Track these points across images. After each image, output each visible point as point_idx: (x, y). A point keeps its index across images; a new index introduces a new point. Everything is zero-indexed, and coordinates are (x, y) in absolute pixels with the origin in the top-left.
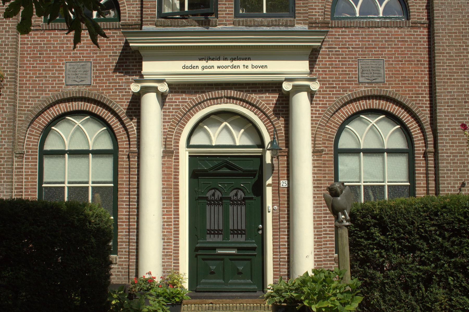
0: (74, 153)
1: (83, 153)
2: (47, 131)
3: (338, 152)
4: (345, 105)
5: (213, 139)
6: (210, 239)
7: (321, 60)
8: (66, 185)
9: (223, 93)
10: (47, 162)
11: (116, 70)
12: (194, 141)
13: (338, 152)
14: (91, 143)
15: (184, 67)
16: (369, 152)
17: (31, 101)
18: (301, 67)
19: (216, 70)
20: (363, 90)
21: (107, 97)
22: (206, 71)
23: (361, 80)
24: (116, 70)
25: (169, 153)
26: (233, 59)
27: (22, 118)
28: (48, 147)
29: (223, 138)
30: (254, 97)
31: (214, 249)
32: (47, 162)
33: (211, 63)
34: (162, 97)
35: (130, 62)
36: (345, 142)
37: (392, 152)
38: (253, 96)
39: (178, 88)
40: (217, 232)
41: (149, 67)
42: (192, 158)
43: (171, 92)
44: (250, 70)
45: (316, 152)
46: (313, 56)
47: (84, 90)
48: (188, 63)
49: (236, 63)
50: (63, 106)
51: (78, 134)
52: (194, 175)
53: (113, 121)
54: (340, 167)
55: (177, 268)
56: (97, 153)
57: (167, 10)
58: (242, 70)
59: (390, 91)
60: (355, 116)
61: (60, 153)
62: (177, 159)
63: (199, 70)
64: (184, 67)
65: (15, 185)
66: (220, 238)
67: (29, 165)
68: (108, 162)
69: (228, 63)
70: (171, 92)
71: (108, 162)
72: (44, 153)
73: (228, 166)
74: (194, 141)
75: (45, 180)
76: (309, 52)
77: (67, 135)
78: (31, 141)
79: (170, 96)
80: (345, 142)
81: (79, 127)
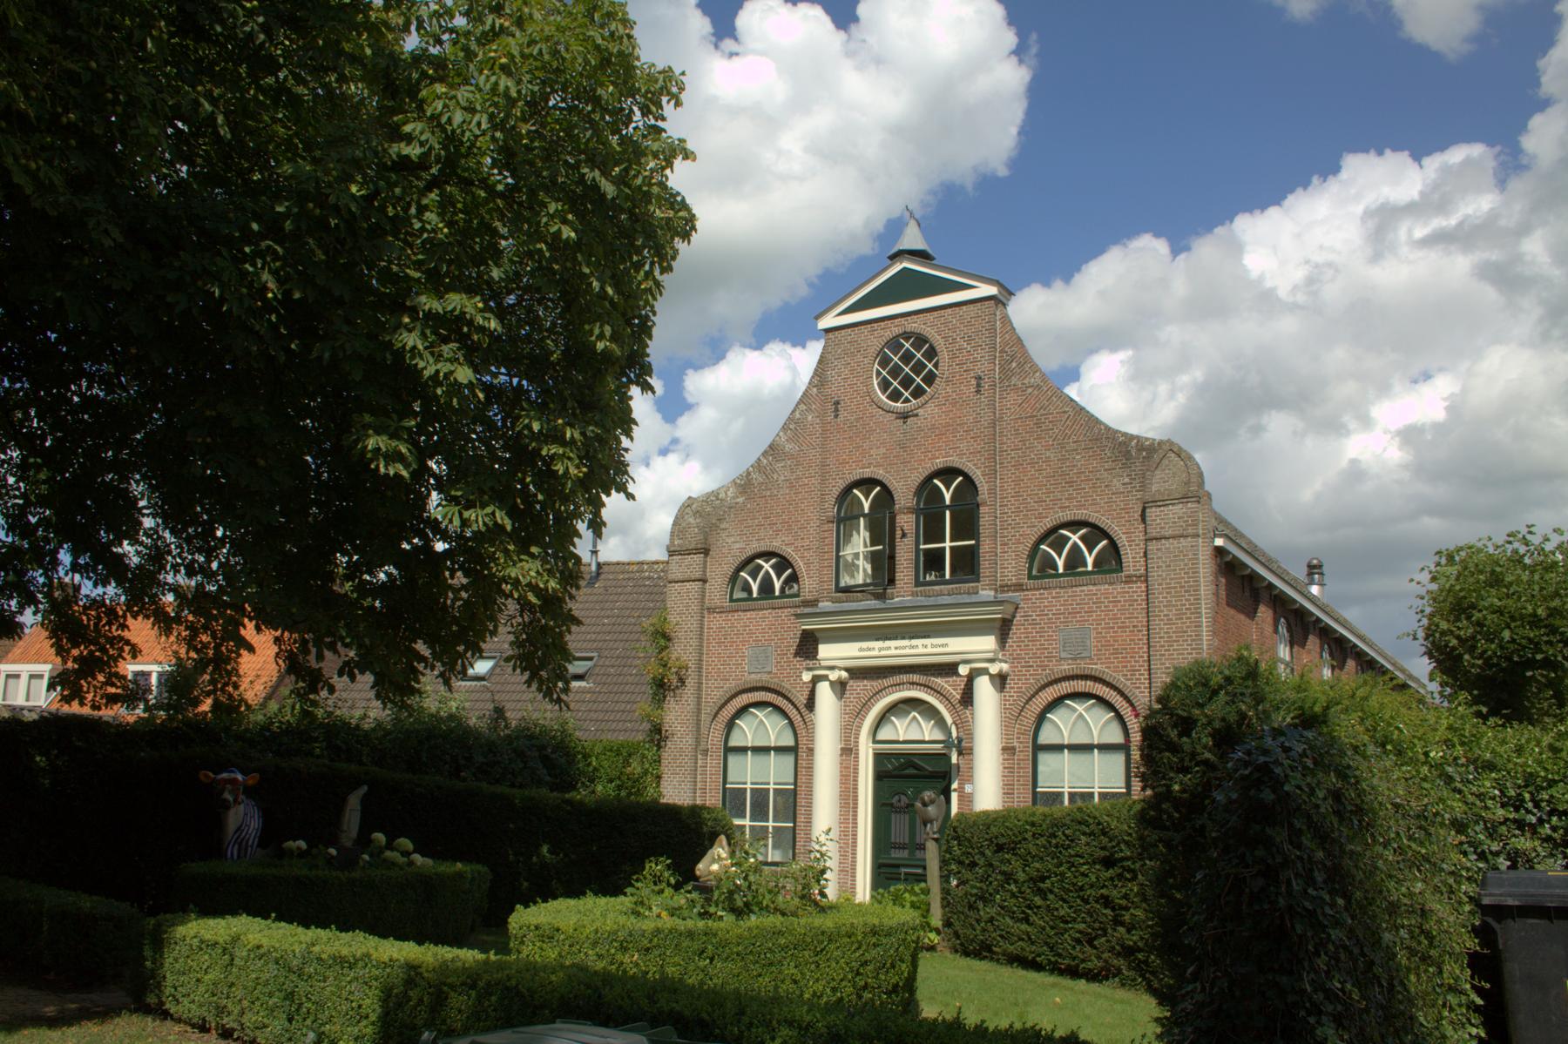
0: (1074, 748)
1: (765, 750)
2: (730, 725)
3: (1038, 748)
4: (1037, 693)
5: (901, 732)
6: (897, 854)
7: (1016, 632)
8: (772, 786)
9: (905, 678)
10: (732, 759)
11: (797, 654)
12: (882, 735)
13: (1038, 748)
14: (1095, 733)
15: (861, 650)
16: (1074, 748)
17: (714, 691)
18: (986, 643)
19: (893, 652)
20: (1066, 668)
21: (786, 685)
22: (884, 653)
23: (1063, 655)
24: (797, 654)
25: (848, 751)
26: (912, 638)
27: (707, 710)
28: (732, 743)
29: (913, 732)
30: (939, 681)
31: (898, 866)
32: (732, 759)
33: (888, 643)
34: (840, 687)
35: (807, 645)
36: (1046, 736)
37: (1105, 748)
38: (939, 680)
39: (858, 673)
40: (903, 847)
41: (826, 651)
42: (879, 758)
43: (851, 678)
44: (929, 650)
45: (1008, 750)
46: (1003, 629)
47: (764, 678)
48: (865, 644)
49: (914, 642)
50: (745, 696)
51: (1080, 724)
52: (880, 776)
53: (793, 713)
54: (1041, 768)
55: (854, 886)
56: (1105, 748)
57: (846, 580)
58: (921, 650)
59: (1098, 668)
60: (742, 711)
61: (1058, 748)
62: (857, 757)
63: (875, 653)
64: (861, 650)
65: (699, 785)
66: (905, 854)
67: (713, 763)
68: (789, 760)
69: (905, 642)
70: (851, 678)
71: (1118, 760)
72: (729, 750)
73: (916, 767)
74: (882, 735)
75: (730, 779)
76: (998, 625)
77: (1064, 725)
78: (715, 737)
79: (851, 683)
80: (1046, 736)
81: (1081, 715)
